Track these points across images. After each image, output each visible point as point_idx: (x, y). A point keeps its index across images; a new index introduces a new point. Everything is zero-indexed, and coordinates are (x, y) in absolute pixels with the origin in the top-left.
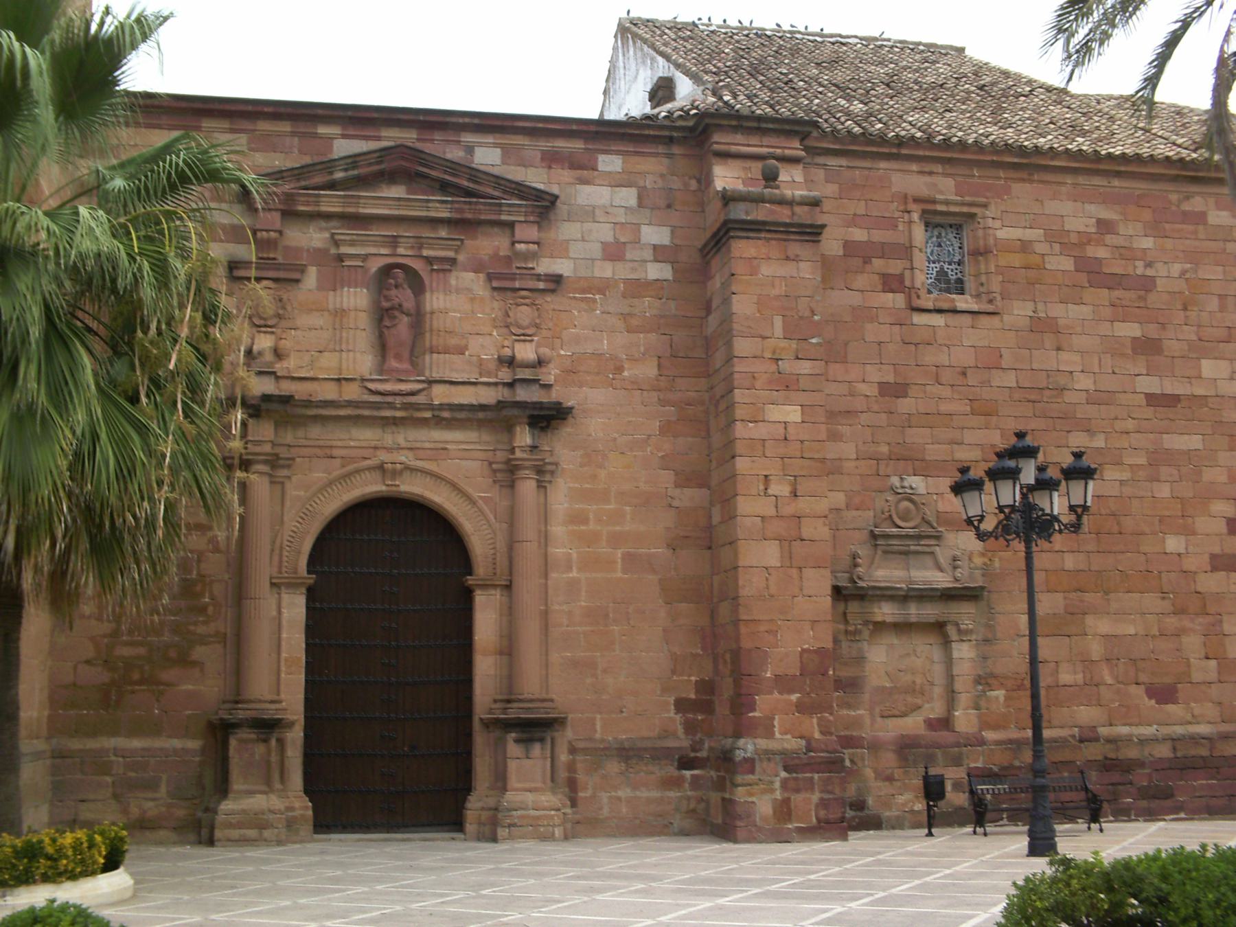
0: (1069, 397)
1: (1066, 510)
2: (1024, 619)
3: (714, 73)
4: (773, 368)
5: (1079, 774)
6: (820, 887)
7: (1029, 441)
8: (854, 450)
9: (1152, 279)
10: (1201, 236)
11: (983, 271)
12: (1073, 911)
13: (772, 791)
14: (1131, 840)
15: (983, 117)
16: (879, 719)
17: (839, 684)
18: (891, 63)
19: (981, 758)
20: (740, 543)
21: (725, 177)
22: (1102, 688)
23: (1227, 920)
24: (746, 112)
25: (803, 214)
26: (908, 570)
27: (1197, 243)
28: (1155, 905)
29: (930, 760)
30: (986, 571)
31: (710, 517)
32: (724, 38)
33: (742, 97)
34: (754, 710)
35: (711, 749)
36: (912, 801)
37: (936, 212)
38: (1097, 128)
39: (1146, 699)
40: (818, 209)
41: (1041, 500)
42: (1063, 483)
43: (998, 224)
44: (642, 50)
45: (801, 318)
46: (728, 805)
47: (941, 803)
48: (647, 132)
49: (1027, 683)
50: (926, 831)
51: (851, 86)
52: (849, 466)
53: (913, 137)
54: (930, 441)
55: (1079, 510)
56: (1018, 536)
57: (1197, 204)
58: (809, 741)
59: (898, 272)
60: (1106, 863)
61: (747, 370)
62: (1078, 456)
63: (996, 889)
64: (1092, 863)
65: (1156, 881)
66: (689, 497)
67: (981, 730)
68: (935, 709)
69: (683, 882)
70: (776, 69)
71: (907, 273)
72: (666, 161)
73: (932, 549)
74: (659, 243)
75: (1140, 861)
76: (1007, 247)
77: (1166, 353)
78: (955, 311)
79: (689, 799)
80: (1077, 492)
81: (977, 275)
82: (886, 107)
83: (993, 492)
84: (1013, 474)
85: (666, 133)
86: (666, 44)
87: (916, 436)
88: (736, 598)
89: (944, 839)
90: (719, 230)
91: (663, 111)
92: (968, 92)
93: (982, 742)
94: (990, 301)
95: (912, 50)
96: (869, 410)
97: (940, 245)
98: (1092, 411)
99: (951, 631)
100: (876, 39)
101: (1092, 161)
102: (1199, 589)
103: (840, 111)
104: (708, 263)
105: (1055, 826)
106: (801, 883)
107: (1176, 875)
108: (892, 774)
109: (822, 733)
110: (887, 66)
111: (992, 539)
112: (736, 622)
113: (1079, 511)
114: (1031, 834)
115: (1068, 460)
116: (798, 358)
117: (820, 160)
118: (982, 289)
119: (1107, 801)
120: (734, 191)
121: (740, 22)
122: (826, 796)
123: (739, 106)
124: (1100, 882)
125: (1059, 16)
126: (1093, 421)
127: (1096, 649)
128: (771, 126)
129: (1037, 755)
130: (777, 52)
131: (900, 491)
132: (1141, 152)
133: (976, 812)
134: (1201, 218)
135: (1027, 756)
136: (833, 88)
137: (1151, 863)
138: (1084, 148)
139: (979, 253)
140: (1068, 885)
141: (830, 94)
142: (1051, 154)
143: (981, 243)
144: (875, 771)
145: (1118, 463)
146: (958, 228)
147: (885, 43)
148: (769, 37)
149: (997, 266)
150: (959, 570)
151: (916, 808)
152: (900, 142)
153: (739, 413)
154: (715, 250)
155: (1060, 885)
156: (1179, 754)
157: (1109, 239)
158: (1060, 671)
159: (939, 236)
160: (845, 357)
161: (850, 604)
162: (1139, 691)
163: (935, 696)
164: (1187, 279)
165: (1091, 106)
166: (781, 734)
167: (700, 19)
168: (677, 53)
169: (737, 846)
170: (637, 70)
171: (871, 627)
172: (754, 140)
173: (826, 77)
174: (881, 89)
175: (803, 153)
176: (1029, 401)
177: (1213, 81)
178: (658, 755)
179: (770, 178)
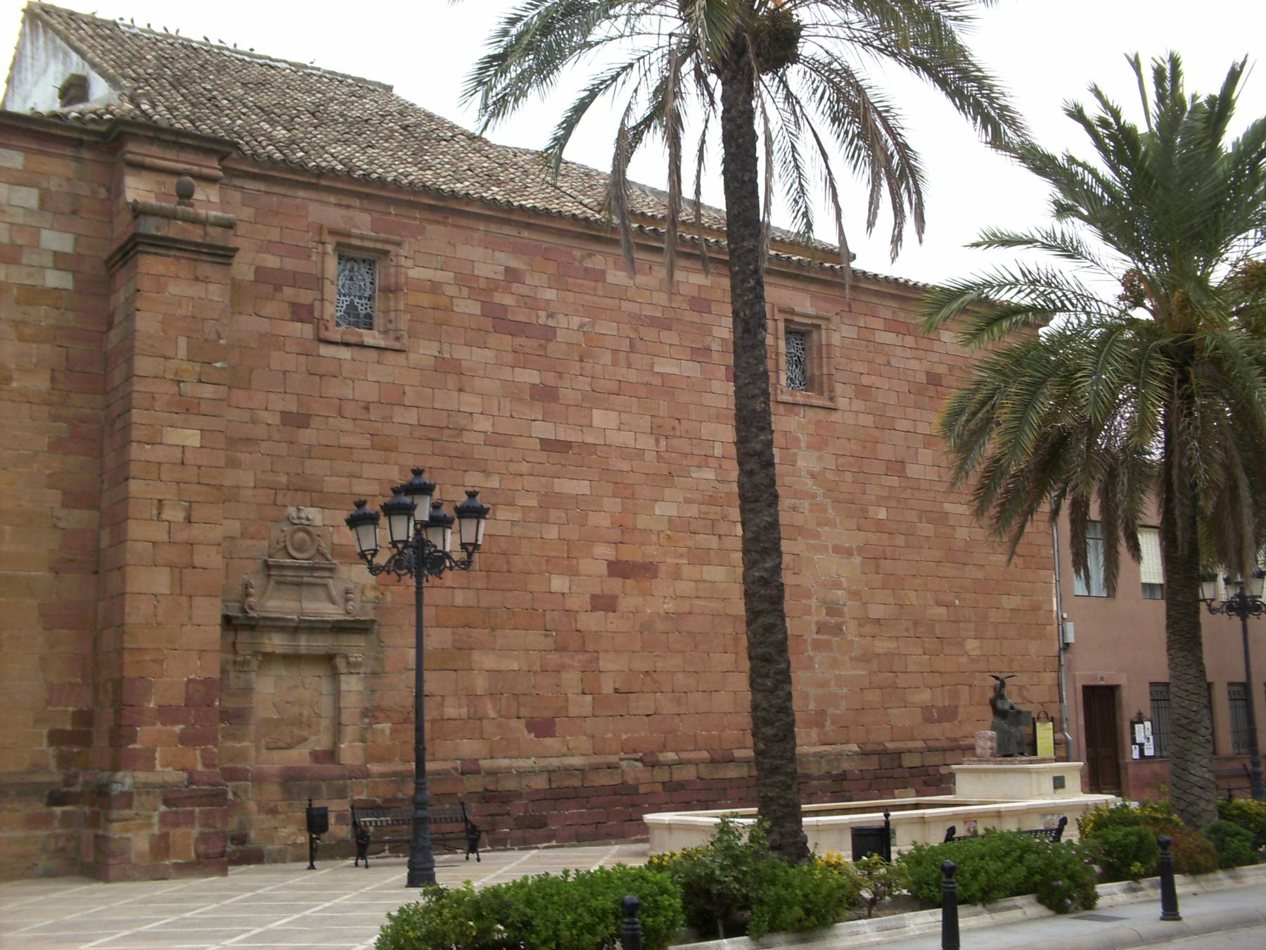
0: (468, 437)
1: (459, 548)
2: (413, 652)
3: (133, 79)
4: (174, 389)
5: (460, 807)
6: (194, 925)
7: (426, 478)
8: (253, 478)
9: (553, 330)
10: (600, 293)
11: (392, 308)
12: (444, 939)
13: (150, 825)
14: (506, 868)
15: (404, 157)
16: (264, 751)
17: (225, 715)
18: (319, 92)
19: (365, 791)
20: (128, 568)
21: (137, 189)
22: (485, 721)
23: (582, 938)
24: (164, 124)
25: (215, 236)
26: (300, 601)
27: (596, 299)
28: (519, 929)
29: (314, 792)
30: (378, 605)
31: (99, 541)
32: (147, 44)
33: (161, 108)
34: (134, 742)
35: (86, 783)
36: (295, 833)
37: (350, 246)
38: (512, 180)
39: (526, 732)
40: (231, 232)
41: (434, 537)
42: (457, 521)
43: (410, 263)
44: (54, 42)
45: (206, 340)
46: (101, 842)
47: (324, 836)
48: (54, 131)
49: (413, 716)
50: (308, 864)
51: (276, 111)
52: (246, 494)
53: (333, 169)
54: (329, 473)
55: (470, 548)
56: (410, 571)
57: (597, 262)
58: (191, 772)
59: (307, 303)
60: (476, 891)
61: (147, 389)
62: (472, 495)
63: (372, 921)
64: (463, 892)
65: (521, 907)
66: (76, 518)
67: (366, 762)
68: (321, 741)
69: (45, 929)
70: (199, 84)
71: (317, 305)
72: (73, 165)
73: (325, 581)
74: (60, 250)
75: (508, 888)
76: (418, 287)
77: (561, 401)
78: (362, 346)
79: (57, 837)
80: (468, 530)
81: (386, 312)
82: (309, 136)
83: (388, 527)
84: (408, 510)
85: (76, 135)
86: (82, 40)
87: (317, 467)
88: (121, 625)
89: (325, 871)
90: (127, 243)
91: (74, 111)
92: (392, 131)
93: (366, 775)
94: (397, 339)
95: (341, 82)
96: (270, 439)
97: (351, 279)
98: (489, 452)
99: (340, 663)
100: (305, 67)
101: (504, 211)
102: (579, 627)
103: (263, 135)
104: (113, 276)
105: (435, 857)
106: (175, 922)
107: (540, 900)
108: (276, 806)
109: (205, 765)
110: (314, 95)
111: (384, 573)
112: (120, 651)
113: (470, 548)
114: (411, 865)
115: (462, 499)
116: (200, 381)
117: (238, 182)
118: (389, 326)
119: (486, 831)
120: (145, 204)
121: (166, 29)
122: (207, 830)
123: (157, 117)
124: (469, 910)
125: (480, 69)
126: (489, 462)
127: (481, 684)
128: (189, 142)
129: (420, 788)
130: (202, 66)
131: (296, 521)
132: (550, 207)
133: (358, 844)
134: (600, 276)
135: (410, 789)
136: (258, 111)
137: (518, 890)
138: (498, 198)
139: (390, 290)
140: (440, 914)
141: (254, 117)
142: (466, 200)
143: (393, 280)
144: (259, 805)
145: (511, 504)
146: (371, 264)
147: (314, 72)
148: (195, 49)
149: (406, 305)
150: (351, 603)
151: (299, 841)
152: (320, 172)
153: (136, 433)
154: (121, 263)
155: (432, 915)
156: (554, 785)
157: (516, 287)
158: (445, 704)
159: (352, 270)
160: (250, 384)
161: (239, 634)
162: (520, 725)
163: (322, 728)
164: (584, 332)
165: (508, 157)
166: (162, 766)
167: (121, 19)
168: (94, 52)
169: (109, 886)
170: (47, 65)
171: (260, 658)
172: (171, 154)
173: (251, 99)
174: (306, 118)
175: (221, 174)
176: (429, 439)
177: (614, 150)
178: (25, 791)
179: (185, 195)
